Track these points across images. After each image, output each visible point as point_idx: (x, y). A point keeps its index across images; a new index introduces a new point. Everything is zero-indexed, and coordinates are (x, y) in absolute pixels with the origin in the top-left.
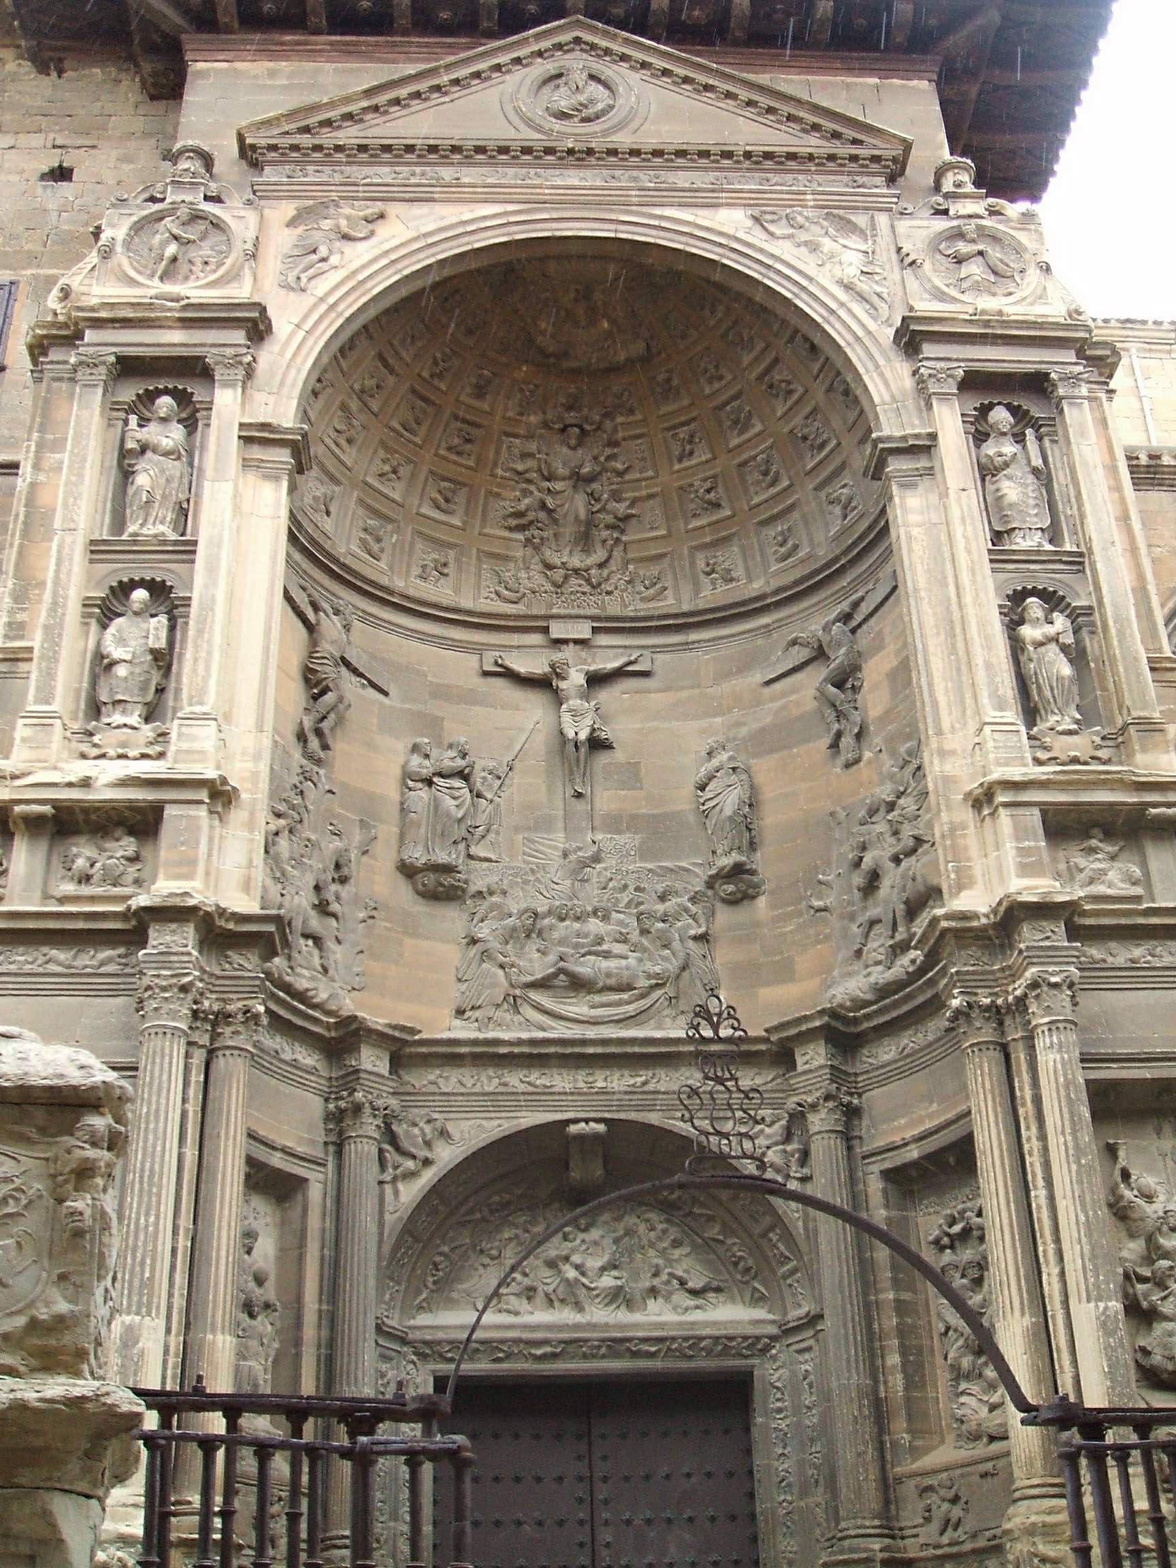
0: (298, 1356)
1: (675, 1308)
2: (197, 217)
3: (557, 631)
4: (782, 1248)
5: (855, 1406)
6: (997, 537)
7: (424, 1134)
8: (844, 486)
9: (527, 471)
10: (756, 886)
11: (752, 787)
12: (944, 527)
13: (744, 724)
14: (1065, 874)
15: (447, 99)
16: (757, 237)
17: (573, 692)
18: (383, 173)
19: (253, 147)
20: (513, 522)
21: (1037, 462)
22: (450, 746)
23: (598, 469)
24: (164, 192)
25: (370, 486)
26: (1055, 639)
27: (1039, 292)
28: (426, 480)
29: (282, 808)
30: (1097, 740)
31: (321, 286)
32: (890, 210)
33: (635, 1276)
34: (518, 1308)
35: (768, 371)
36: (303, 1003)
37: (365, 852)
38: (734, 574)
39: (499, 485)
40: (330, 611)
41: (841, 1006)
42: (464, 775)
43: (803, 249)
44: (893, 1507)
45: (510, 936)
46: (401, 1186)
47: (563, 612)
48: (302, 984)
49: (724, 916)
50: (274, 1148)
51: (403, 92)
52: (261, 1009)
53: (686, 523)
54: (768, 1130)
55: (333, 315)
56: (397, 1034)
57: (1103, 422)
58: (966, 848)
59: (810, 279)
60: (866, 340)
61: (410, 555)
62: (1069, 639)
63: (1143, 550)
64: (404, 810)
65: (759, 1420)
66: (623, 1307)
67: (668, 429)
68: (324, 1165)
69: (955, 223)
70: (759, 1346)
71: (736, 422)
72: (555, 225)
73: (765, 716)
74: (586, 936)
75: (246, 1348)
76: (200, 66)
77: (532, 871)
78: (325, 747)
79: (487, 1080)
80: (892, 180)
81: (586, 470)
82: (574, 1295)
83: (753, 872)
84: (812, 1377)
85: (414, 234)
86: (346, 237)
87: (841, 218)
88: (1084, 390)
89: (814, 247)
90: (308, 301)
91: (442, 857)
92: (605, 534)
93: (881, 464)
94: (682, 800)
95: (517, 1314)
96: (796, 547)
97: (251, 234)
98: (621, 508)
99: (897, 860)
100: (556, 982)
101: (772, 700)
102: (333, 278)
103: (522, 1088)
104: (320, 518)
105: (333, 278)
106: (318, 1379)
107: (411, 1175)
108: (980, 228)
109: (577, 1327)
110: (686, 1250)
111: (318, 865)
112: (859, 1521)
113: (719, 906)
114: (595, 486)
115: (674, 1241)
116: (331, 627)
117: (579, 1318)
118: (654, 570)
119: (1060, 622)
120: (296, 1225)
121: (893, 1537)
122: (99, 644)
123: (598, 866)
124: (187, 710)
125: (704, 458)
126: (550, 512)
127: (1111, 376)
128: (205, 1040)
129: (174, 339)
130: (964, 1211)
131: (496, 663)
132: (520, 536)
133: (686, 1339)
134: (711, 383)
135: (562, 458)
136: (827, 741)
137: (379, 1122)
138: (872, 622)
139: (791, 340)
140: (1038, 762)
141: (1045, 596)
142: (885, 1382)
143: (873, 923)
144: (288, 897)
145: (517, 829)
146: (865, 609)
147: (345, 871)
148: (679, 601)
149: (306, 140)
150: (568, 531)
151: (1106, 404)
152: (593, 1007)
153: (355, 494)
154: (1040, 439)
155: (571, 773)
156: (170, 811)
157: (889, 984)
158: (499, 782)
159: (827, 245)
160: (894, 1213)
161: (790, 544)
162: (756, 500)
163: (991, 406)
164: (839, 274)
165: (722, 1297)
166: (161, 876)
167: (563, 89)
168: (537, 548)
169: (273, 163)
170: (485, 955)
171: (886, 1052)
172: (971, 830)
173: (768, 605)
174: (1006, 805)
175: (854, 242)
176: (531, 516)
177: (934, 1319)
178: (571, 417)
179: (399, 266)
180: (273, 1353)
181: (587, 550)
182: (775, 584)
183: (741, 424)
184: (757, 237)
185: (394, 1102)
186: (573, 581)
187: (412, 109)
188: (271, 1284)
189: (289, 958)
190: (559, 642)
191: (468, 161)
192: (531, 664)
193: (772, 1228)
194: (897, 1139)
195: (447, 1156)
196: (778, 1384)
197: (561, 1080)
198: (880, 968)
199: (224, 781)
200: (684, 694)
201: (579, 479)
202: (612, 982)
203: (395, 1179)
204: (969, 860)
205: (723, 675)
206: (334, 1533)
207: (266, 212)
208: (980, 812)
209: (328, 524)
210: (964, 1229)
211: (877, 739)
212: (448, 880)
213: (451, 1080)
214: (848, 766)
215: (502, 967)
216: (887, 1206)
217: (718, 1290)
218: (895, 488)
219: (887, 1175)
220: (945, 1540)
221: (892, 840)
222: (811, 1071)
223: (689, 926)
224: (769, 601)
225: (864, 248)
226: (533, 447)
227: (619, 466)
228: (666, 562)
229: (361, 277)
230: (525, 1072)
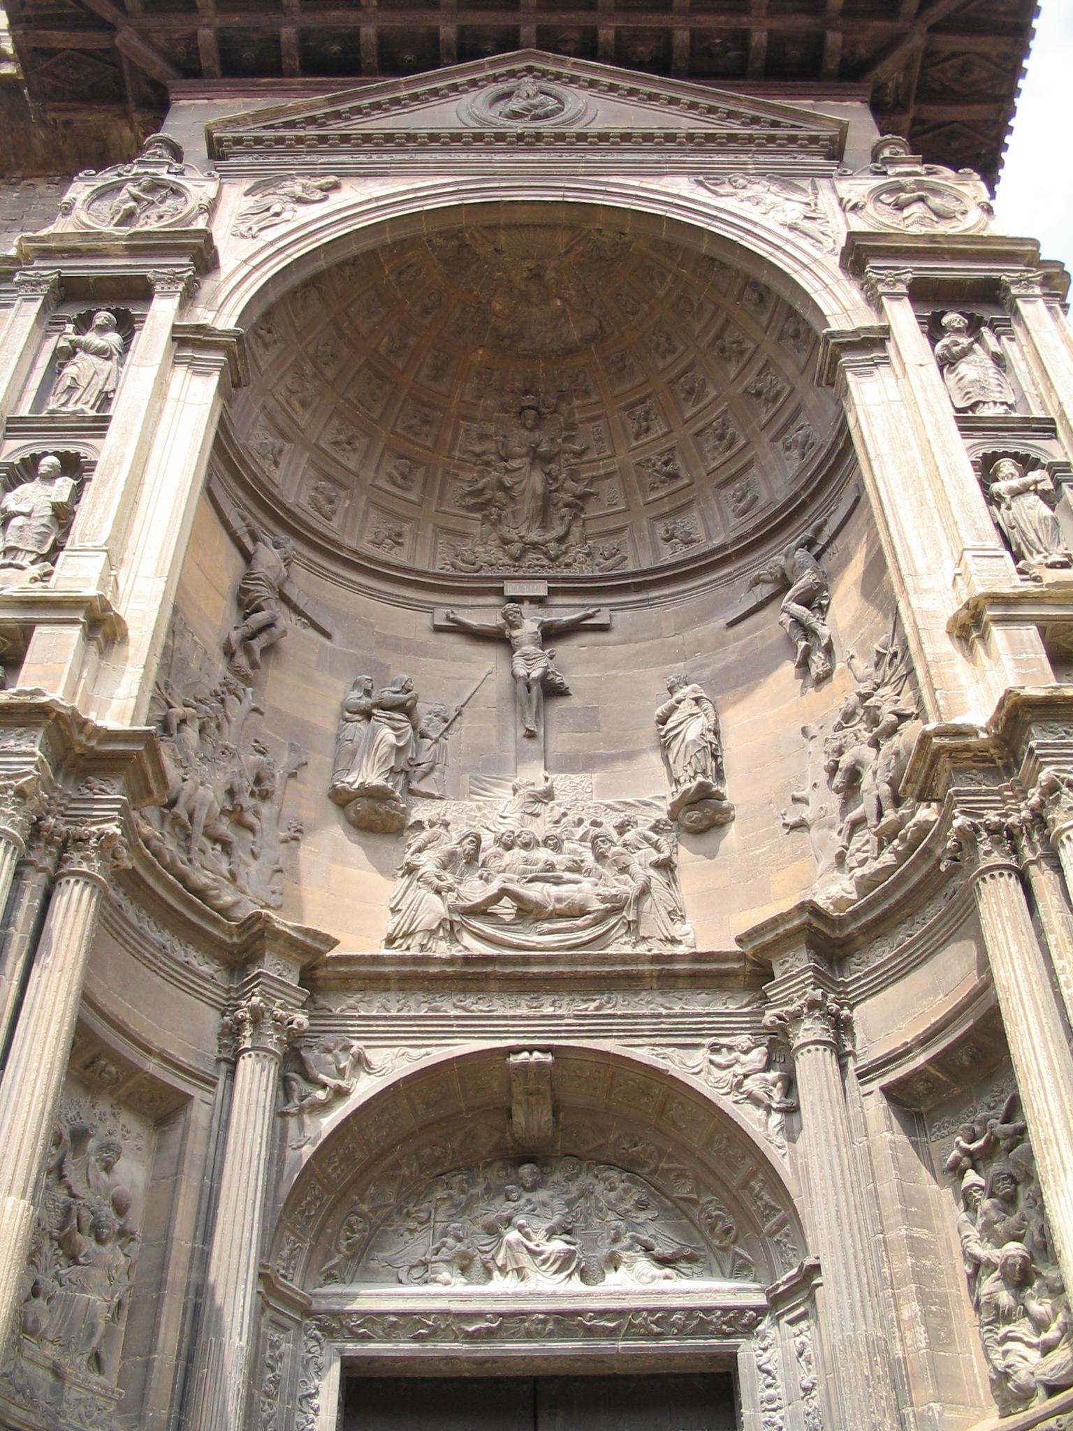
0: (159, 1302)
1: (638, 1278)
3: (511, 589)
4: (766, 1197)
5: (866, 1364)
9: (484, 453)
10: (727, 811)
13: (706, 665)
17: (526, 639)
25: (323, 450)
28: (382, 455)
33: (592, 1243)
35: (718, 337)
39: (456, 467)
40: (270, 543)
46: (307, 1119)
50: (149, 1051)
53: (645, 497)
54: (743, 1058)
56: (309, 941)
58: (955, 677)
59: (755, 224)
60: (813, 267)
67: (623, 408)
68: (214, 1085)
73: (730, 654)
76: (182, 103)
77: (479, 808)
79: (417, 1006)
93: (835, 359)
98: (580, 488)
101: (736, 640)
104: (266, 465)
106: (182, 1333)
107: (324, 1107)
109: (517, 1296)
115: (638, 1202)
116: (268, 558)
117: (521, 1287)
118: (613, 542)
120: (174, 1151)
125: (660, 433)
126: (506, 489)
128: (48, 862)
129: (120, 265)
130: (987, 1119)
131: (448, 617)
132: (478, 516)
133: (652, 1311)
134: (664, 357)
135: (519, 439)
138: (837, 542)
144: (189, 783)
145: (463, 770)
146: (828, 531)
147: (267, 785)
150: (527, 506)
152: (541, 934)
153: (307, 455)
155: (523, 713)
161: (749, 496)
162: (714, 465)
163: (943, 314)
173: (729, 556)
174: (999, 620)
176: (488, 494)
178: (529, 400)
181: (545, 526)
190: (513, 599)
191: (423, 148)
192: (484, 616)
193: (753, 1175)
195: (364, 1088)
196: (768, 1367)
201: (538, 458)
207: (226, 187)
208: (966, 640)
209: (277, 475)
210: (987, 1142)
213: (372, 1005)
215: (438, 891)
217: (691, 1259)
222: (792, 977)
225: (806, 200)
226: (491, 429)
227: (577, 448)
230: (461, 997)
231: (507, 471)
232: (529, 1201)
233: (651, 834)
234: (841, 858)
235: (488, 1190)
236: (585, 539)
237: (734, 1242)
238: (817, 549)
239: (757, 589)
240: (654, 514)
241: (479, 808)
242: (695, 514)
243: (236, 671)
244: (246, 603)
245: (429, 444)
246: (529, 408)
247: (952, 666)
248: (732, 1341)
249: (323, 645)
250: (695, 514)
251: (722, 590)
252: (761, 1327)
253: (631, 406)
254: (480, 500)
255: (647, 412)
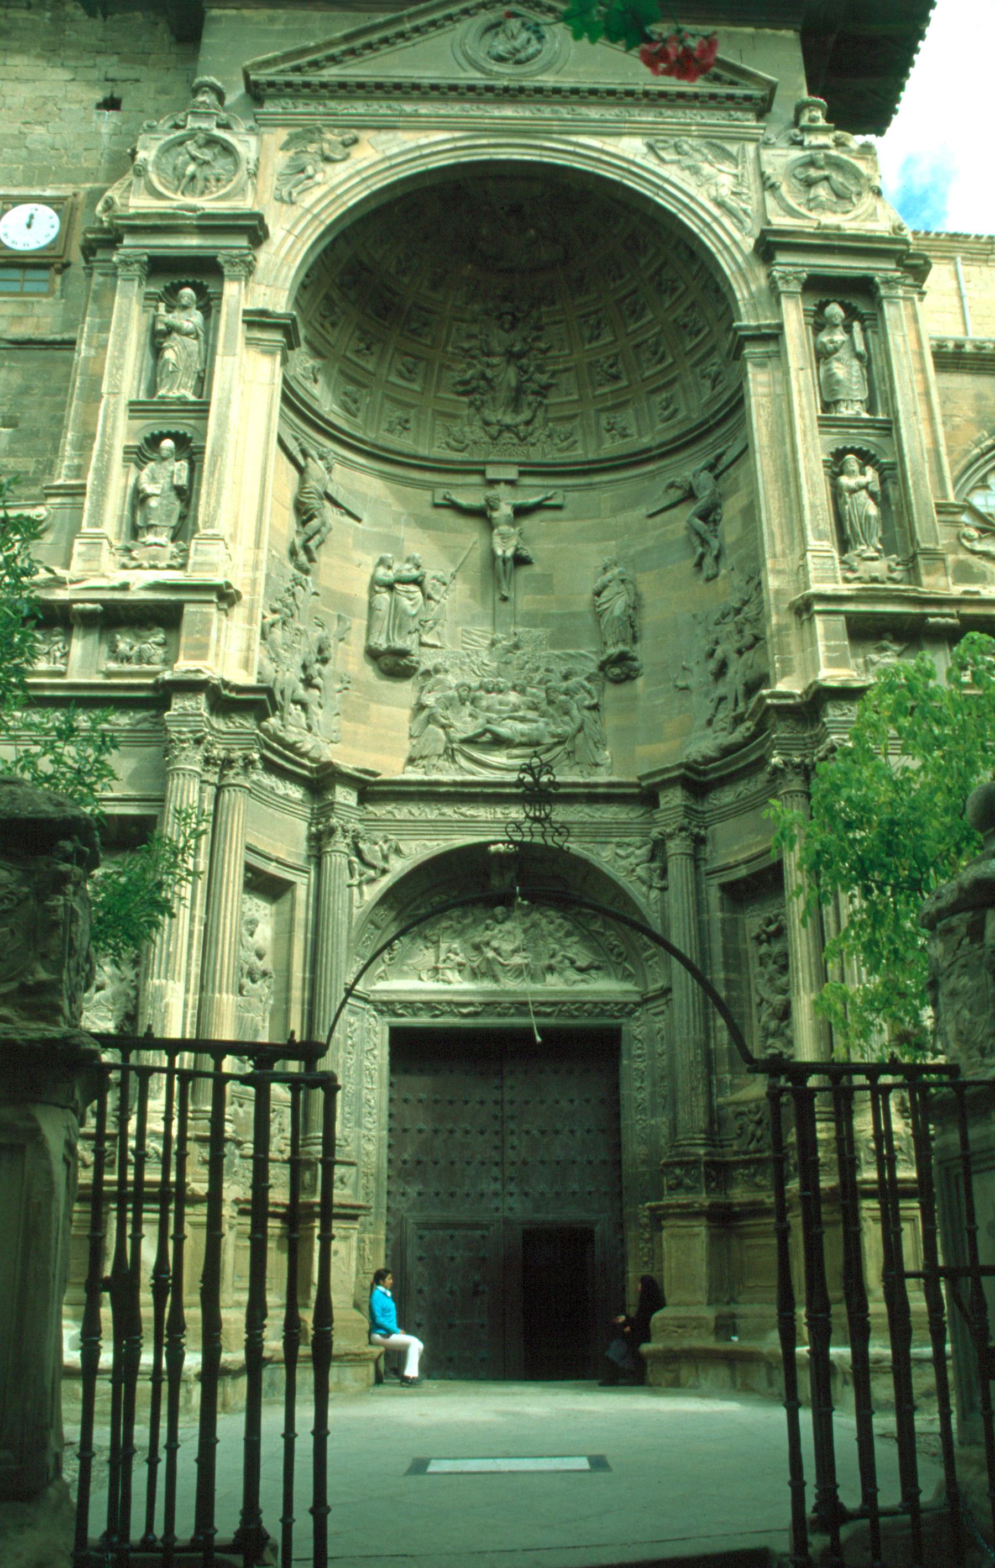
2: (211, 141)
3: (491, 473)
6: (826, 406)
7: (382, 850)
8: (713, 365)
10: (637, 670)
11: (636, 594)
12: (785, 398)
14: (862, 668)
15: (409, 43)
16: (651, 162)
17: (503, 520)
18: (360, 107)
19: (257, 84)
20: (461, 389)
21: (860, 347)
22: (408, 560)
23: (526, 348)
24: (185, 120)
25: (349, 359)
26: (865, 487)
27: (870, 211)
29: (277, 605)
30: (893, 564)
31: (308, 200)
32: (756, 140)
34: (451, 978)
35: (658, 272)
36: (291, 751)
37: (342, 640)
38: (629, 431)
40: (316, 457)
41: (695, 762)
42: (417, 582)
43: (687, 173)
44: (716, 1126)
45: (448, 704)
47: (496, 459)
48: (291, 738)
49: (611, 691)
51: (375, 37)
52: (256, 756)
54: (638, 852)
55: (317, 223)
57: (915, 318)
58: (789, 645)
60: (733, 249)
61: (380, 413)
62: (876, 488)
63: (939, 419)
64: (371, 609)
65: (625, 1062)
66: (528, 979)
69: (808, 152)
70: (626, 1009)
71: (633, 312)
72: (492, 150)
74: (507, 705)
75: (250, 1004)
76: (215, 12)
77: (468, 656)
78: (311, 560)
79: (429, 812)
80: (760, 115)
81: (516, 349)
82: (493, 970)
83: (634, 659)
84: (663, 1033)
85: (378, 157)
86: (328, 160)
87: (719, 147)
88: (900, 292)
89: (695, 171)
90: (296, 211)
91: (399, 644)
92: (531, 398)
94: (583, 602)
95: (450, 983)
96: (676, 411)
97: (252, 156)
98: (544, 379)
99: (740, 652)
100: (484, 739)
102: (317, 192)
103: (456, 817)
105: (317, 192)
107: (371, 881)
108: (827, 157)
109: (493, 993)
110: (575, 939)
111: (305, 649)
112: (690, 1135)
113: (608, 685)
114: (524, 361)
116: (316, 468)
118: (568, 427)
119: (871, 475)
121: (714, 1146)
122: (137, 479)
123: (519, 652)
124: (203, 531)
126: (488, 381)
127: (923, 281)
128: (215, 779)
132: (465, 399)
133: (573, 1003)
135: (499, 339)
136: (695, 559)
137: (349, 840)
138: (731, 470)
139: (676, 247)
140: (847, 580)
141: (860, 454)
142: (715, 1038)
143: (722, 699)
144: (280, 673)
145: (457, 623)
146: (726, 460)
147: (326, 654)
148: (586, 452)
149: (296, 78)
150: (503, 395)
151: (918, 303)
153: (337, 365)
154: (864, 330)
156: (188, 609)
157: (731, 745)
158: (444, 588)
159: (706, 169)
160: (728, 915)
162: (647, 374)
163: (827, 303)
164: (714, 193)
165: (601, 973)
166: (181, 657)
167: (501, 36)
168: (478, 409)
169: (272, 97)
170: (431, 719)
171: (727, 797)
172: (793, 631)
174: (820, 613)
175: (727, 167)
176: (474, 384)
177: (753, 993)
178: (507, 307)
179: (369, 182)
180: (269, 1008)
181: (517, 410)
182: (659, 439)
183: (636, 313)
184: (651, 162)
185: (359, 827)
186: (507, 435)
187: (382, 52)
188: (268, 958)
189: (282, 718)
190: (492, 483)
194: (731, 860)
195: (399, 867)
197: (483, 813)
198: (725, 733)
199: (229, 586)
200: (588, 523)
201: (512, 356)
202: (524, 739)
203: (360, 885)
204: (790, 653)
205: (615, 511)
206: (312, 1135)
211: (730, 560)
212: (404, 662)
214: (708, 579)
216: (722, 910)
217: (598, 968)
218: (750, 368)
219: (724, 887)
220: (752, 1147)
221: (736, 637)
223: (585, 699)
224: (654, 453)
225: (734, 171)
226: (475, 329)
227: (542, 345)
228: (577, 422)
229: (339, 191)
231: (488, 365)
232: (500, 931)
233: (586, 683)
234: (710, 722)
235: (474, 921)
236: (547, 421)
237: (625, 960)
238: (717, 471)
239: (672, 491)
240: (599, 406)
241: (468, 656)
242: (630, 411)
243: (300, 568)
244: (303, 513)
245: (428, 342)
246: (508, 313)
247: (788, 636)
248: (620, 1021)
249: (357, 529)
250: (630, 411)
251: (646, 484)
252: (637, 1014)
253: (588, 315)
254: (468, 388)
255: (599, 322)
